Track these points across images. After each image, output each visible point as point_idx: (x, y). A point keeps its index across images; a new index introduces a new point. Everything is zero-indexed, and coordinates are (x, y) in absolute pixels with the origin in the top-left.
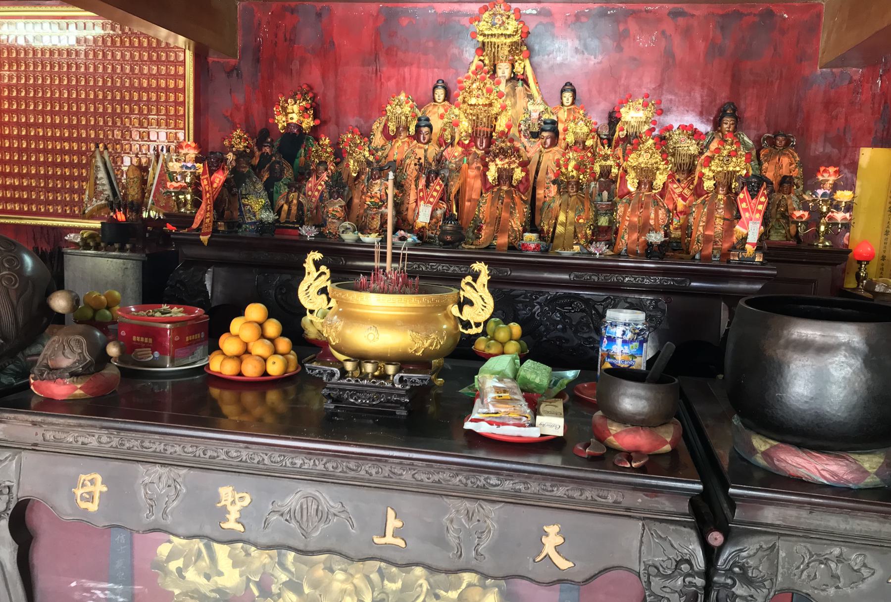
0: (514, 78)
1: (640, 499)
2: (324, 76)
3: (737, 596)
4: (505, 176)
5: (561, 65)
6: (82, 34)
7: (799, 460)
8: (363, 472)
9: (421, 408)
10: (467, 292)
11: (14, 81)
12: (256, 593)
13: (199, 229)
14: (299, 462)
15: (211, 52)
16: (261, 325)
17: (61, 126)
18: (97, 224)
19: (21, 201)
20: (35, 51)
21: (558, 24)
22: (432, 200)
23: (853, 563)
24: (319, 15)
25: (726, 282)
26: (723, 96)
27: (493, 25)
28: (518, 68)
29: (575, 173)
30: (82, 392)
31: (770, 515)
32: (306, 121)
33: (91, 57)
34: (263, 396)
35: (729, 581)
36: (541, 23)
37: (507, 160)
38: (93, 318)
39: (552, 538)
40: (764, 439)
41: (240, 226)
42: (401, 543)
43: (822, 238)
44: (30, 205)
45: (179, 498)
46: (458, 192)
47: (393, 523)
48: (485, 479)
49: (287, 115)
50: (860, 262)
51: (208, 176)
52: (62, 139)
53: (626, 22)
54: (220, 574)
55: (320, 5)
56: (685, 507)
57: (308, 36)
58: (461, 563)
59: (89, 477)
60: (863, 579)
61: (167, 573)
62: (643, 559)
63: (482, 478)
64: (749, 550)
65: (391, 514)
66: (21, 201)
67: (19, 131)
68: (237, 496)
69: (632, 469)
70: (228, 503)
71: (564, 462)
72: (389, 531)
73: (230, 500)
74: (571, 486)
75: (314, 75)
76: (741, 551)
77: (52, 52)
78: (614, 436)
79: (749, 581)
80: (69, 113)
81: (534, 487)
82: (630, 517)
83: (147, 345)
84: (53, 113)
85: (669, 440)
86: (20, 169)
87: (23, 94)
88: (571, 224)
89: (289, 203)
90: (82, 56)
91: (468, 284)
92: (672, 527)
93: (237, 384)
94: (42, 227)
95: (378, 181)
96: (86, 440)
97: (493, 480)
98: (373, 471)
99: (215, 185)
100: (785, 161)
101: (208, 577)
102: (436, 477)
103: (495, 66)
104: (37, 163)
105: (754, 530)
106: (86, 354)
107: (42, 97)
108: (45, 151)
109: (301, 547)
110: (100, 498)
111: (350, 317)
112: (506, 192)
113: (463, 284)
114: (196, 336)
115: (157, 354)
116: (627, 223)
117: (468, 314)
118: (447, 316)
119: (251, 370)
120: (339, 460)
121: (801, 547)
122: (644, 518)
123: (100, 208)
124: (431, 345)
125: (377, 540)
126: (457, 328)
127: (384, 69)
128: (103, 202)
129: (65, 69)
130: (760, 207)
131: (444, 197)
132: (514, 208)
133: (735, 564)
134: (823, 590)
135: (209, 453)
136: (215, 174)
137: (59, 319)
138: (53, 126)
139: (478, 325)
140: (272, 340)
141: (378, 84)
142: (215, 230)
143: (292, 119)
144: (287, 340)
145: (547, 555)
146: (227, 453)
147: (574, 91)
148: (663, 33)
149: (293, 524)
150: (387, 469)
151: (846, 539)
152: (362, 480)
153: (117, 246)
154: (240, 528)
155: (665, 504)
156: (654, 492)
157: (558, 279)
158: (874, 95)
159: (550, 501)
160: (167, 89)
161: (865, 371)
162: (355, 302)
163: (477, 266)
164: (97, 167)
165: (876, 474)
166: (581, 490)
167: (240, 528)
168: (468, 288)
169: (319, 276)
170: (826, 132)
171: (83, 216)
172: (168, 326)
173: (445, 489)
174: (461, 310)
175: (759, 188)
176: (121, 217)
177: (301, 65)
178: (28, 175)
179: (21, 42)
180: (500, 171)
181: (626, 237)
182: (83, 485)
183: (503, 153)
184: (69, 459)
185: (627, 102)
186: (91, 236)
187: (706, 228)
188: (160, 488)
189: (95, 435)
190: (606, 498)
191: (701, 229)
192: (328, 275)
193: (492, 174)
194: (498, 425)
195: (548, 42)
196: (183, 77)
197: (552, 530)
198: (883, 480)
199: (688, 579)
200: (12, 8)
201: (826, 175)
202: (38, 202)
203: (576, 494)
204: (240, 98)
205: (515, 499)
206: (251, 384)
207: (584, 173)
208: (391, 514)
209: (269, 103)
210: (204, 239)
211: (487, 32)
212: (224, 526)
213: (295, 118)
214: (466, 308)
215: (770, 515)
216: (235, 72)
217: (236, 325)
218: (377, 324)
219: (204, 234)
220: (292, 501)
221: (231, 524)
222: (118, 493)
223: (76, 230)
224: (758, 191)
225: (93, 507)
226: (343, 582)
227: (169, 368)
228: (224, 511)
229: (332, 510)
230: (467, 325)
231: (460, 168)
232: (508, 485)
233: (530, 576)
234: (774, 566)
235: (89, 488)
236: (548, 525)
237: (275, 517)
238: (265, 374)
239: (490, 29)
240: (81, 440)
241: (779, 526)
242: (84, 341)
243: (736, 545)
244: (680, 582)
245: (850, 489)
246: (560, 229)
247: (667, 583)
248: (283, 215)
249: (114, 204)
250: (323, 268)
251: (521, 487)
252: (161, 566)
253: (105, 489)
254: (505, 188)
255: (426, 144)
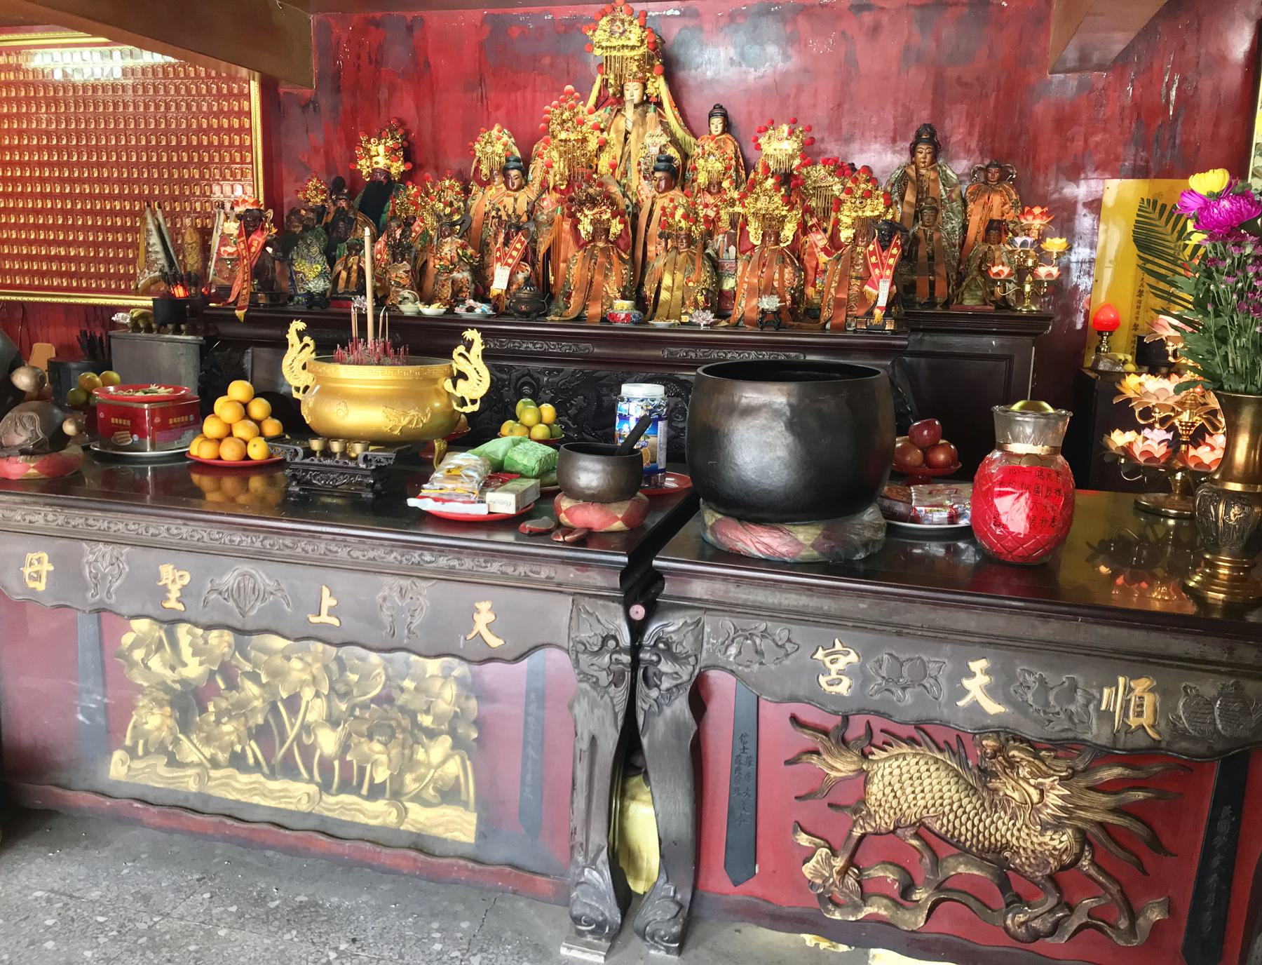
0: (645, 102)
1: (571, 574)
2: (418, 108)
3: (663, 674)
4: (601, 229)
5: (712, 82)
6: (129, 62)
7: (658, 520)
8: (299, 550)
9: (387, 486)
10: (459, 364)
11: (54, 126)
12: (222, 686)
13: (235, 302)
14: (237, 539)
15: (282, 83)
16: (245, 405)
17: (108, 181)
18: (148, 302)
19: (69, 275)
20: (75, 87)
21: (707, 27)
22: (510, 261)
23: (777, 638)
24: (410, 29)
25: (847, 356)
26: (923, 115)
27: (612, 33)
28: (650, 90)
29: (683, 224)
30: (35, 471)
31: (698, 589)
32: (395, 165)
33: (140, 92)
34: (246, 481)
35: (654, 658)
36: (686, 27)
37: (596, 210)
38: (87, 402)
39: (484, 616)
40: (779, 526)
41: (291, 298)
42: (335, 622)
43: (1028, 301)
44: (78, 279)
45: (123, 577)
46: (549, 250)
47: (328, 602)
48: (420, 556)
49: (371, 157)
50: (1100, 333)
51: (244, 238)
52: (112, 197)
53: (795, 21)
54: (185, 665)
55: (410, 15)
56: (616, 581)
57: (398, 54)
58: (394, 643)
59: (36, 556)
60: (787, 655)
61: (133, 664)
62: (573, 636)
63: (416, 554)
64: (671, 626)
65: (326, 592)
66: (69, 275)
67: (63, 188)
68: (178, 574)
69: (564, 542)
70: (169, 582)
71: (517, 539)
72: (324, 610)
73: (171, 578)
74: (505, 561)
75: (406, 107)
76: (666, 625)
77: (94, 88)
78: (565, 512)
79: (675, 658)
80: (118, 164)
81: (468, 563)
82: (561, 592)
83: (124, 428)
84: (99, 165)
85: (620, 516)
86: (66, 235)
87: (64, 142)
88: (678, 288)
89: (349, 270)
90: (130, 92)
91: (461, 354)
92: (600, 602)
93: (215, 468)
94: (95, 307)
95: (449, 239)
96: (33, 519)
97: (428, 557)
98: (310, 548)
99: (253, 249)
100: (996, 200)
101: (173, 668)
102: (371, 554)
103: (622, 87)
104: (85, 228)
105: (682, 604)
106: (39, 432)
107: (87, 145)
108: (93, 213)
109: (239, 626)
110: (47, 577)
111: (330, 392)
112: (602, 249)
113: (455, 355)
114: (184, 419)
115: (136, 437)
116: (746, 286)
117: (463, 389)
118: (438, 393)
119: (229, 453)
120: (275, 537)
121: (728, 623)
122: (575, 594)
123: (154, 281)
124: (410, 422)
125: (314, 619)
126: (451, 406)
127: (492, 94)
128: (157, 274)
129: (111, 109)
130: (891, 261)
131: (528, 256)
132: (610, 270)
133: (659, 640)
134: (748, 666)
135: (151, 531)
136: (253, 236)
137: (20, 396)
138: (100, 181)
139: (473, 402)
140: (259, 423)
141: (485, 114)
142: (253, 303)
143: (377, 163)
144: (277, 421)
145: (479, 634)
146: (168, 530)
147: (725, 116)
148: (843, 33)
149: (231, 603)
150: (323, 546)
151: (774, 613)
152: (298, 557)
153: (170, 326)
154: (180, 607)
155: (595, 579)
156: (583, 565)
157: (263, 328)
158: (1123, 108)
159: (482, 577)
160: (230, 130)
161: (787, 434)
162: (332, 376)
163: (471, 334)
164: (148, 231)
165: (813, 546)
166: (515, 565)
167: (180, 607)
168: (461, 359)
169: (303, 348)
170: (1059, 160)
171: (137, 292)
172: (146, 406)
173: (379, 567)
174: (455, 386)
175: (891, 237)
176: (179, 292)
177: (391, 94)
178: (75, 243)
179: (58, 76)
180: (593, 222)
181: (743, 304)
182: (31, 564)
183: (592, 202)
184: (16, 537)
185: (766, 129)
186: (142, 316)
187: (837, 290)
188: (104, 567)
189: (43, 516)
190: (539, 573)
191: (832, 291)
192: (312, 347)
193: (586, 227)
194: (444, 501)
195: (696, 52)
196: (249, 115)
197: (484, 606)
198: (821, 553)
199: (615, 656)
200: (46, 35)
201: (1030, 218)
202: (88, 276)
203: (510, 570)
204: (319, 138)
205: (449, 576)
206: (230, 469)
207: (696, 221)
208: (326, 592)
209: (352, 143)
210: (240, 314)
211: (604, 44)
212: (167, 605)
213: (381, 162)
214: (460, 382)
215: (698, 589)
216: (311, 106)
217: (220, 403)
218: (359, 398)
219: (241, 308)
220: (229, 580)
221: (172, 603)
222: (67, 571)
223: (126, 309)
224: (890, 241)
225: (41, 586)
226: (302, 670)
227: (149, 453)
228: (165, 589)
229: (269, 589)
230: (463, 402)
231: (553, 220)
232: (442, 562)
233: (461, 654)
234: (699, 642)
235: (37, 567)
236: (480, 601)
237: (214, 596)
238: (247, 457)
239: (608, 40)
240: (28, 518)
241: (707, 600)
242: (37, 418)
243: (661, 620)
244: (607, 658)
245: (786, 562)
246: (664, 295)
247: (595, 660)
248: (342, 284)
249: (171, 277)
250: (307, 339)
251: (455, 563)
252: (126, 656)
253: (51, 568)
254: (601, 244)
255: (516, 190)
